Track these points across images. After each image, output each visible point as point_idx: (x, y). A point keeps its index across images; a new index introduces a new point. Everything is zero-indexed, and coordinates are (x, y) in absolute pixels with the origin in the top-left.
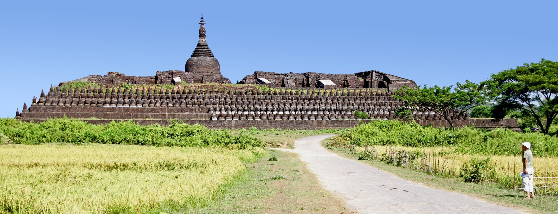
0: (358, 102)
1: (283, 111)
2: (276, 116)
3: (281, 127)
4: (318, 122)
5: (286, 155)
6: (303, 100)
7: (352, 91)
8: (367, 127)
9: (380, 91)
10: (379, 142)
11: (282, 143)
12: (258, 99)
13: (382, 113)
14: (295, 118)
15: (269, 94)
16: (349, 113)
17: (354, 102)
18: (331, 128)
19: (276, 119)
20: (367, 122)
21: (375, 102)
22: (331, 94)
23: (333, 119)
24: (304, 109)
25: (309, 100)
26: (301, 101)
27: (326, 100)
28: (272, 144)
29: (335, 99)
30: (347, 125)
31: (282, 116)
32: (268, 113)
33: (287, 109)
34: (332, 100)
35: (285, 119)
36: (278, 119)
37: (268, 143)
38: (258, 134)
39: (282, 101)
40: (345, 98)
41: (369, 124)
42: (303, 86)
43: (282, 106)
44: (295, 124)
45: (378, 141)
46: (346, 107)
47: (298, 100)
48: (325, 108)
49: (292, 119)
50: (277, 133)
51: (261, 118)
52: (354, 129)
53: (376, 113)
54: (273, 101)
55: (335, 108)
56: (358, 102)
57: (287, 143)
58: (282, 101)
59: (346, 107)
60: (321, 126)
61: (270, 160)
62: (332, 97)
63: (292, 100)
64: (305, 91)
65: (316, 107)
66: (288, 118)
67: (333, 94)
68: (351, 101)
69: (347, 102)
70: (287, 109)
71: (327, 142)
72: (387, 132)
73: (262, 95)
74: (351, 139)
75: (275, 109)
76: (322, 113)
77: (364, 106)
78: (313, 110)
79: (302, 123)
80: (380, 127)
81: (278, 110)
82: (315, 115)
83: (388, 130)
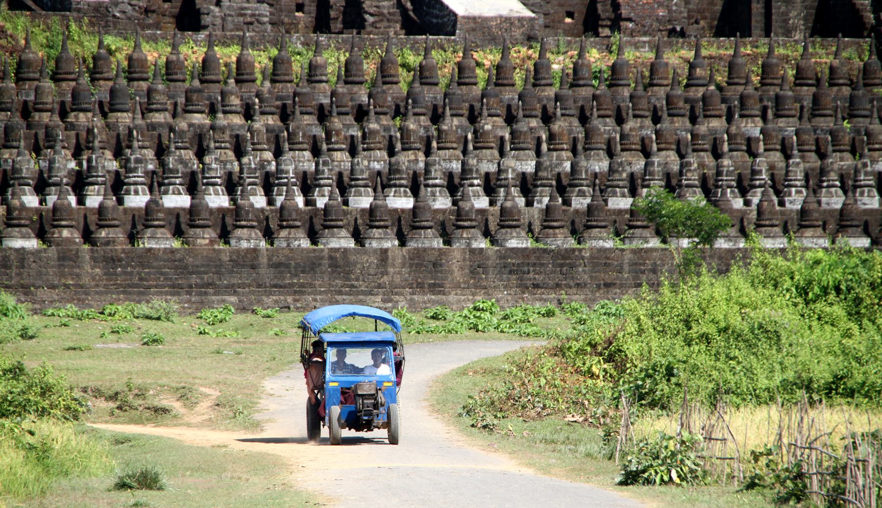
0: (680, 127)
1: (192, 188)
2: (144, 220)
3: (175, 289)
4: (418, 260)
5: (209, 463)
6: (322, 115)
7: (637, 55)
8: (721, 297)
9: (823, 56)
10: (787, 387)
11: (185, 395)
12: (26, 112)
13: (834, 200)
14: (269, 235)
15: (95, 74)
16: (621, 202)
17: (649, 132)
18: (500, 301)
19: (147, 243)
20: (723, 265)
21: (788, 127)
22: (500, 75)
23: (516, 242)
24: (328, 178)
25: (361, 114)
26: (308, 124)
27: (473, 118)
28: (122, 403)
29: (528, 109)
30: (608, 277)
31: (181, 224)
32: (93, 201)
33: (217, 171)
34: (510, 119)
35: (205, 238)
36: (159, 242)
37: (98, 393)
38: (25, 335)
39: (183, 125)
40: (595, 104)
41: (736, 277)
42: (322, 25)
43: (183, 157)
44: (266, 274)
45: (778, 378)
46: (600, 165)
47: (285, 115)
48: (465, 171)
49: (248, 240)
50: (153, 328)
51: (41, 235)
52: (634, 305)
53: (795, 201)
54: (124, 119)
55: (529, 167)
56: (680, 127)
57: (214, 393)
58: (183, 125)
59: (600, 165)
60: (436, 288)
61: (122, 486)
62: (510, 95)
63: (248, 113)
64: (333, 59)
65: (404, 159)
66: (225, 235)
67: (518, 77)
68: (631, 124)
69: (606, 127)
70: (217, 171)
71: (471, 388)
72: (846, 323)
73: (48, 84)
74: (621, 368)
75: (139, 176)
76: (442, 202)
77: (717, 155)
78: (382, 183)
79: (311, 265)
80: (803, 291)
81: (157, 183)
82: (398, 216)
83: (855, 315)
